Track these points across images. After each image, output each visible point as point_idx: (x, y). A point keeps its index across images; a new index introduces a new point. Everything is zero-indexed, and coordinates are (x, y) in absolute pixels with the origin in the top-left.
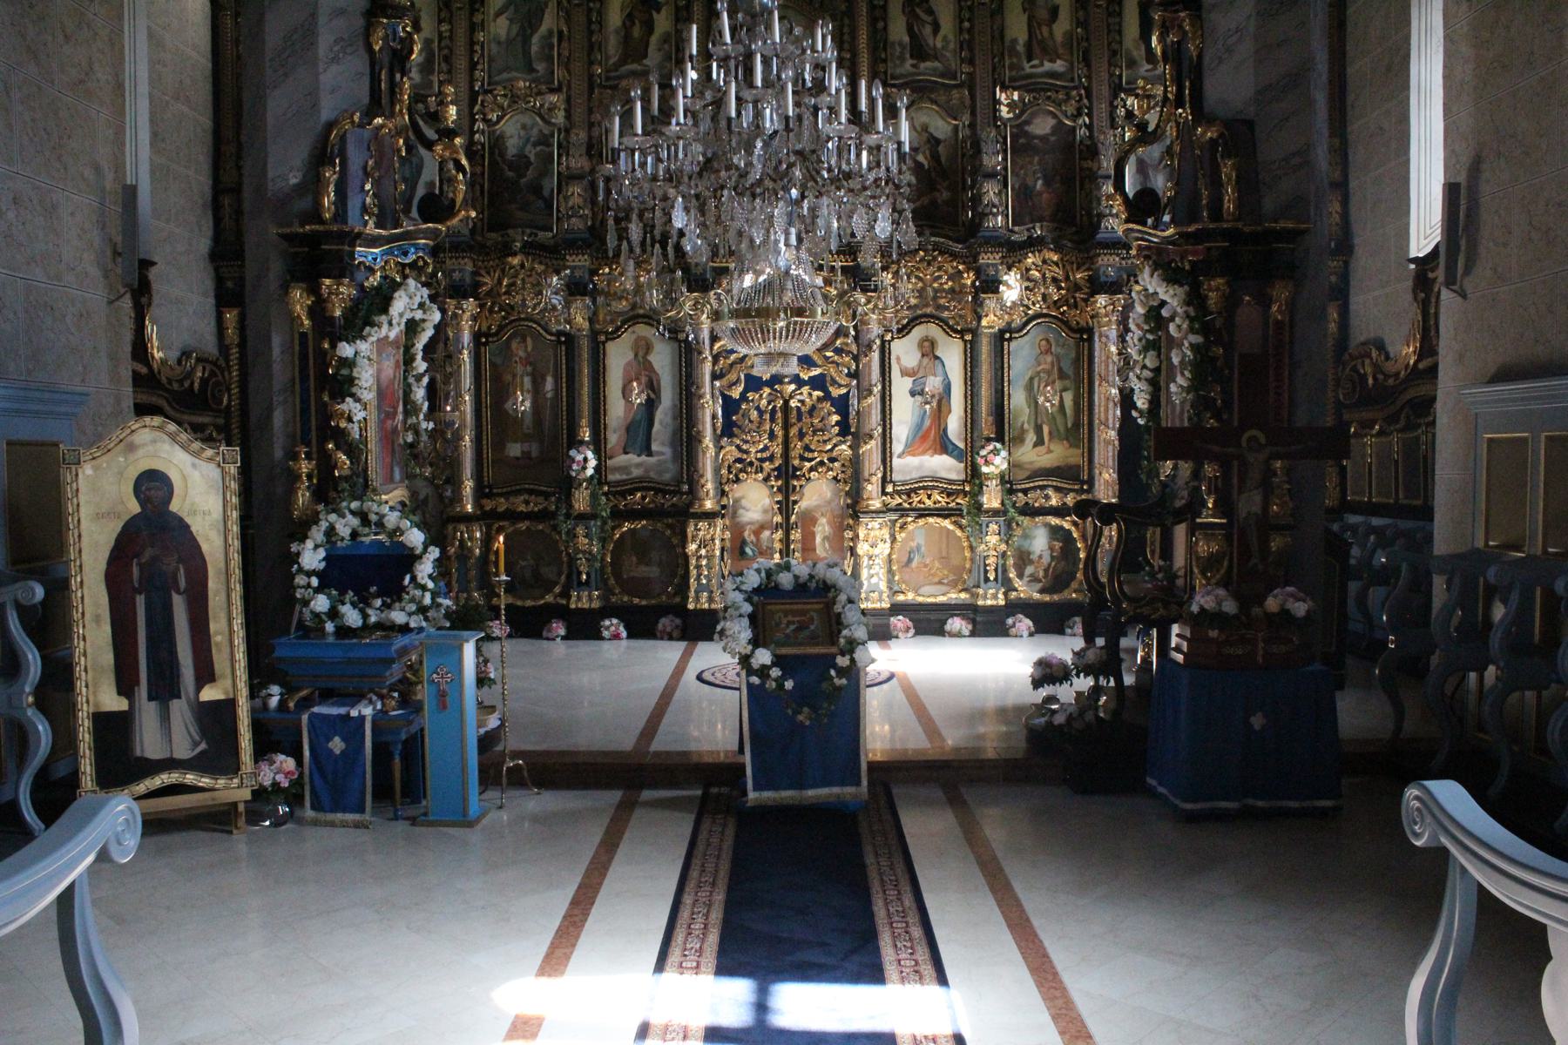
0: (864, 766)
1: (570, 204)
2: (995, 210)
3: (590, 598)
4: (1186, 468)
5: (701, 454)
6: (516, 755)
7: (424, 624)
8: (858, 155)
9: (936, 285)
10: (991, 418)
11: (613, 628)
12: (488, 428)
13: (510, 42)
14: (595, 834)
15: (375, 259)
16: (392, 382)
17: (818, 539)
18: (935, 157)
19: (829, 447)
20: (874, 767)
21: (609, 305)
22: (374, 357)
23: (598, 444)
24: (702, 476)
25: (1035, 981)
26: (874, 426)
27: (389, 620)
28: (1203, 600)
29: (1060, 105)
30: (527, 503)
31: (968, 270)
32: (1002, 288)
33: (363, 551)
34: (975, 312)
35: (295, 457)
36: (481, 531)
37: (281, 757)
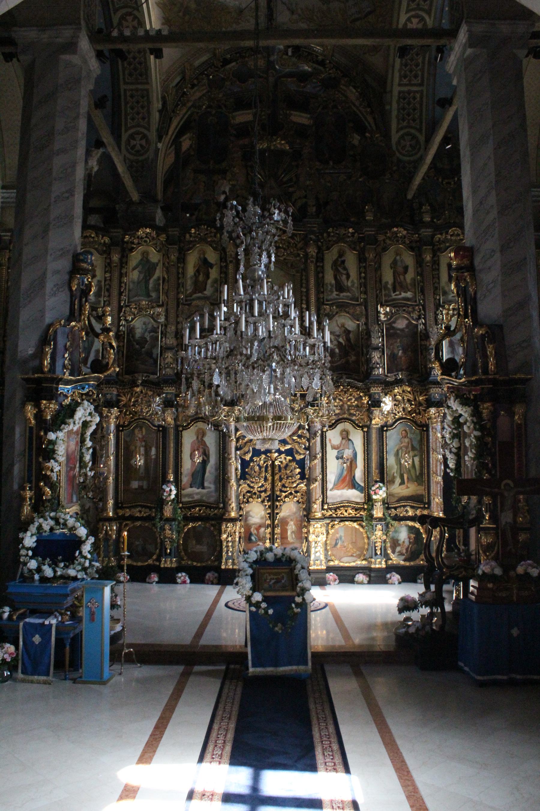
0: (309, 655)
1: (166, 361)
2: (378, 366)
3: (171, 562)
4: (474, 499)
5: (229, 489)
6: (129, 646)
7: (85, 576)
8: (304, 349)
9: (349, 403)
10: (377, 471)
11: (182, 578)
12: (122, 473)
13: (139, 282)
14: (169, 689)
15: (68, 391)
16: (74, 452)
17: (289, 533)
18: (348, 340)
19: (295, 485)
20: (315, 655)
21: (184, 412)
22: (65, 439)
23: (177, 483)
24: (230, 500)
25: (398, 776)
26: (318, 475)
27: (67, 574)
28: (484, 568)
29: (410, 313)
30: (140, 512)
31: (365, 396)
32: (382, 404)
33: (56, 538)
34: (369, 417)
35: (24, 489)
36: (117, 526)
37: (8, 645)
